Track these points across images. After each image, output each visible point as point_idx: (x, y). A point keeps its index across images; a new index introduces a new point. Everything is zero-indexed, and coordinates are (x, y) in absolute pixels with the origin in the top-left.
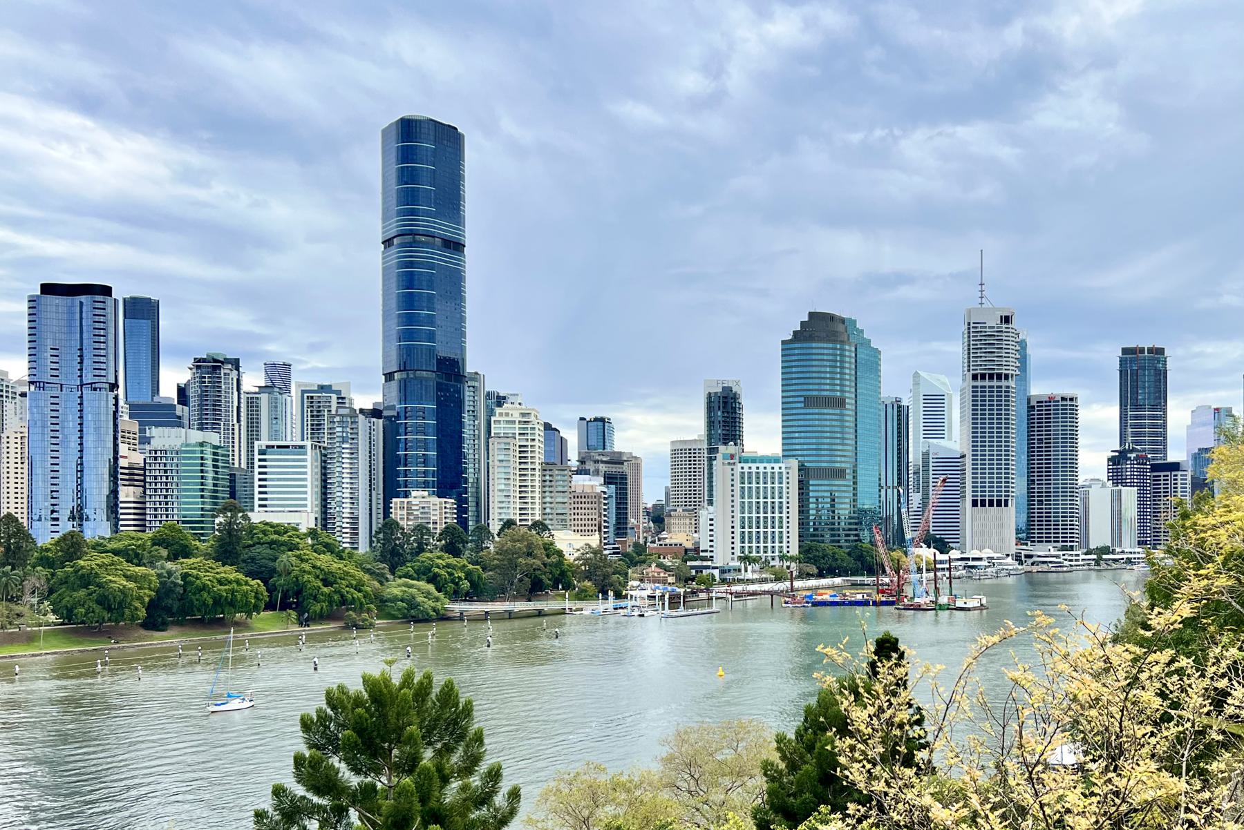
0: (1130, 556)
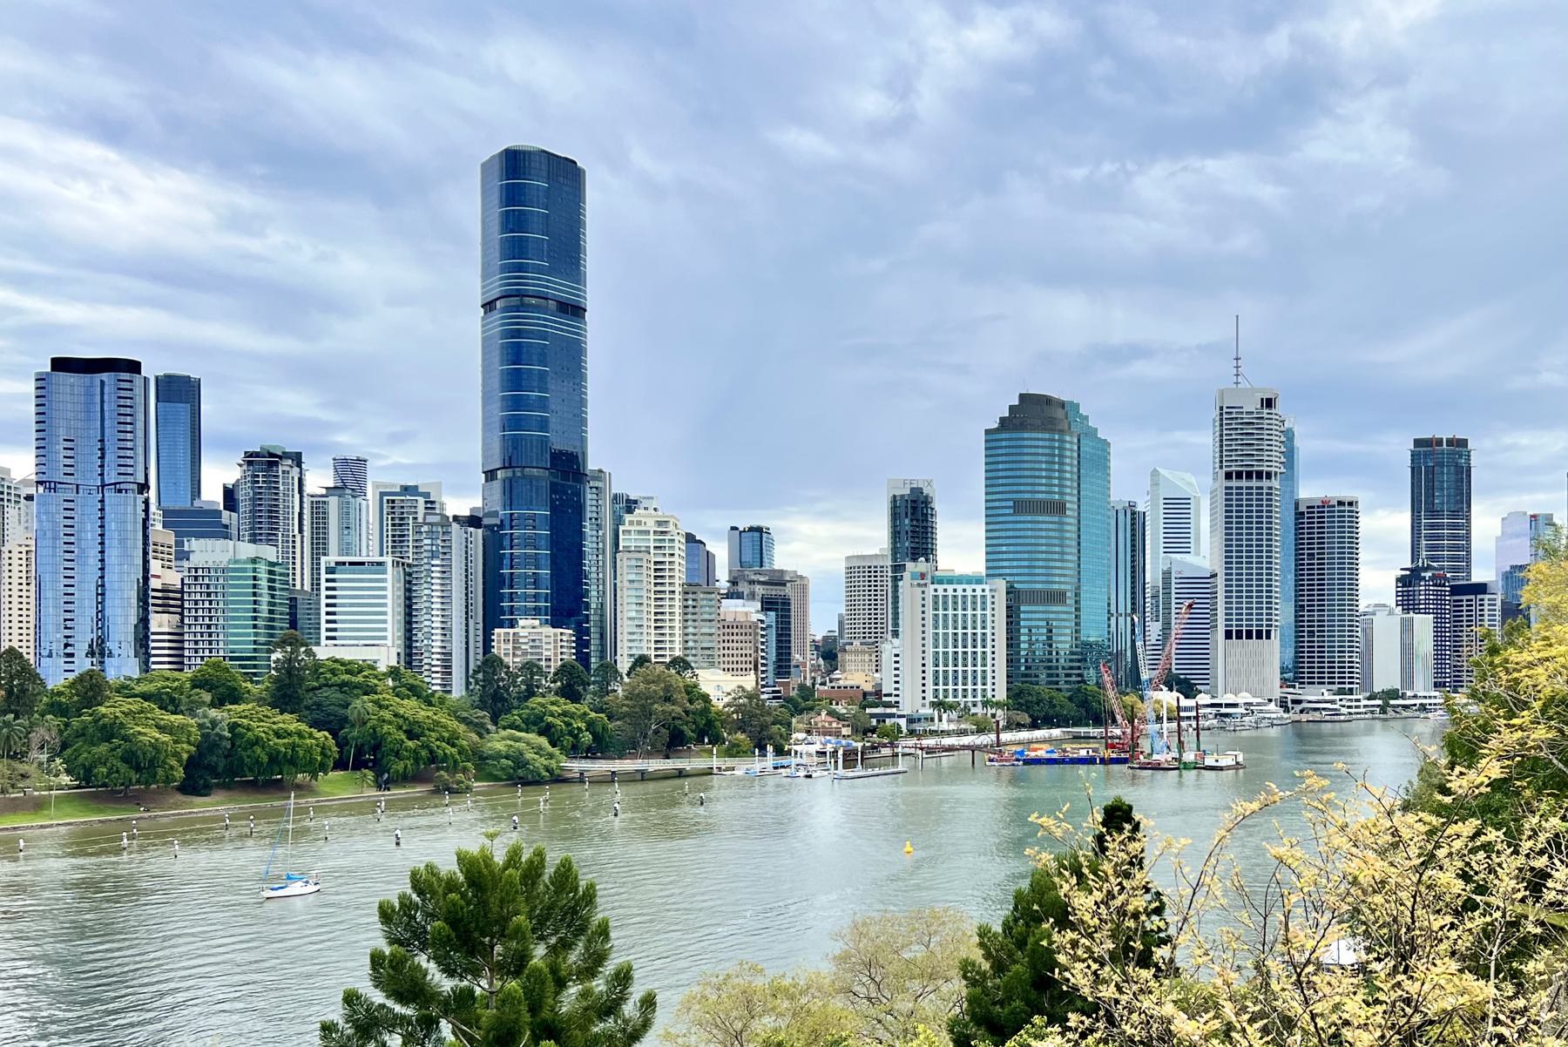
0: (1424, 701)
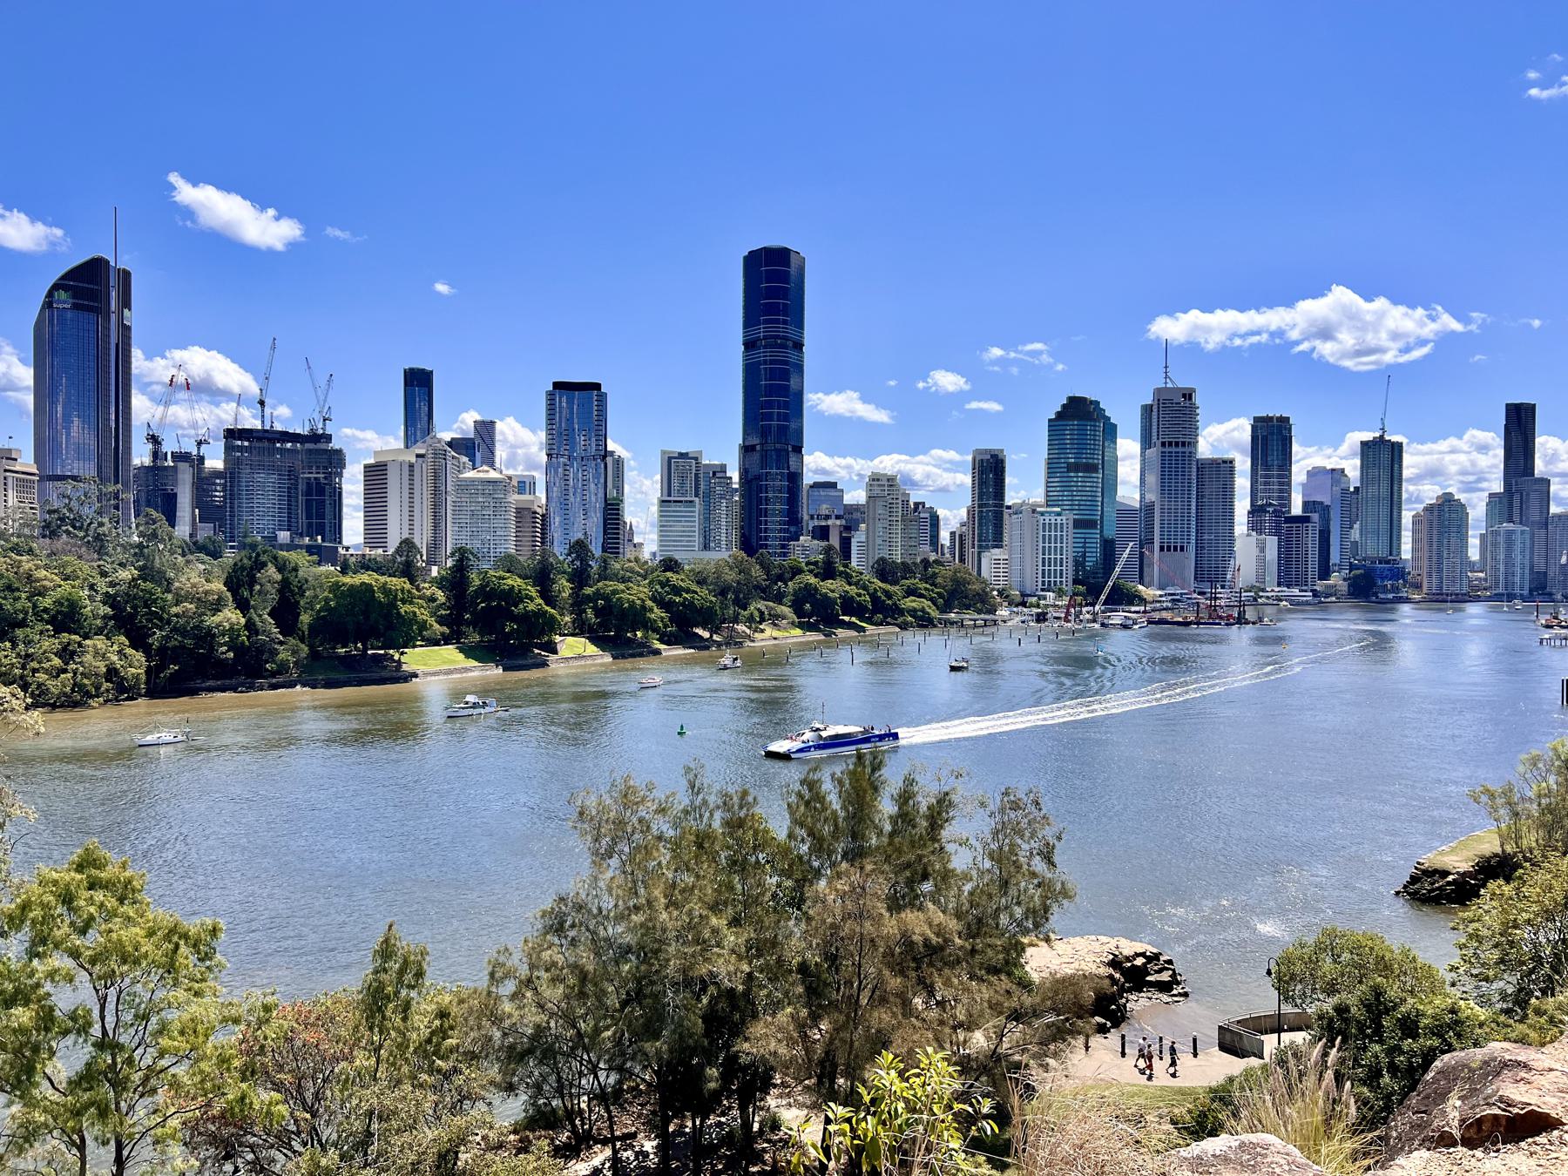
0: (1280, 594)
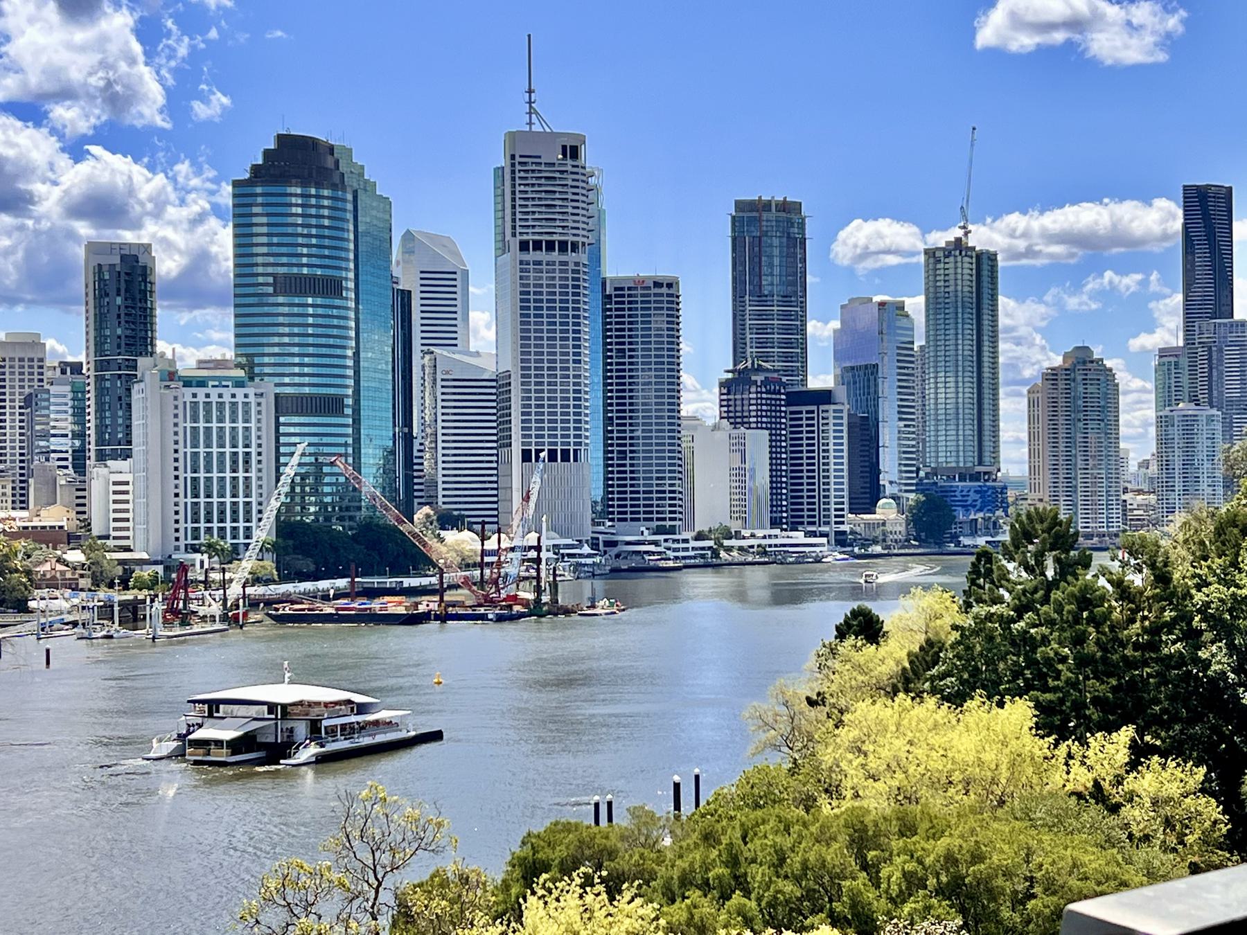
0: (764, 542)
